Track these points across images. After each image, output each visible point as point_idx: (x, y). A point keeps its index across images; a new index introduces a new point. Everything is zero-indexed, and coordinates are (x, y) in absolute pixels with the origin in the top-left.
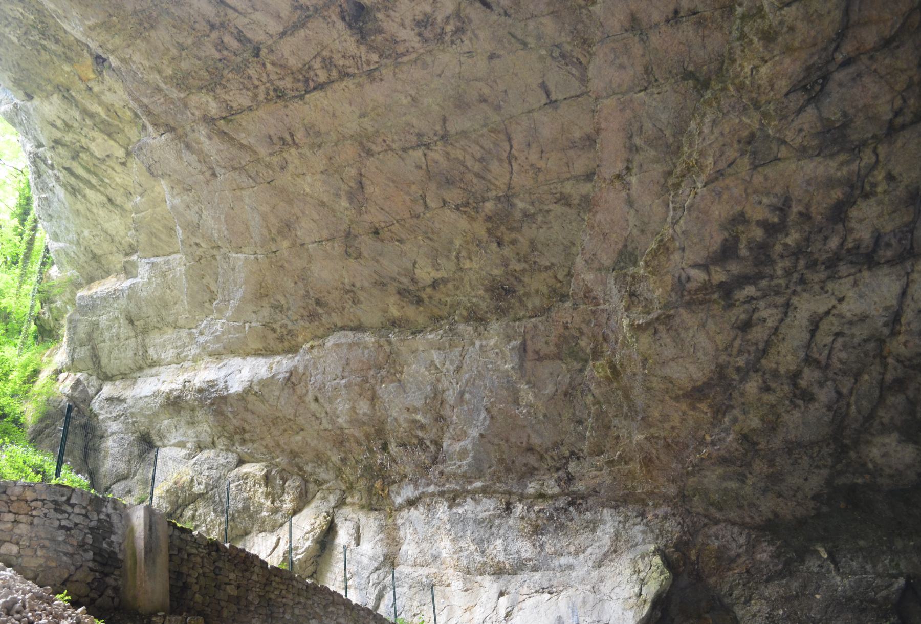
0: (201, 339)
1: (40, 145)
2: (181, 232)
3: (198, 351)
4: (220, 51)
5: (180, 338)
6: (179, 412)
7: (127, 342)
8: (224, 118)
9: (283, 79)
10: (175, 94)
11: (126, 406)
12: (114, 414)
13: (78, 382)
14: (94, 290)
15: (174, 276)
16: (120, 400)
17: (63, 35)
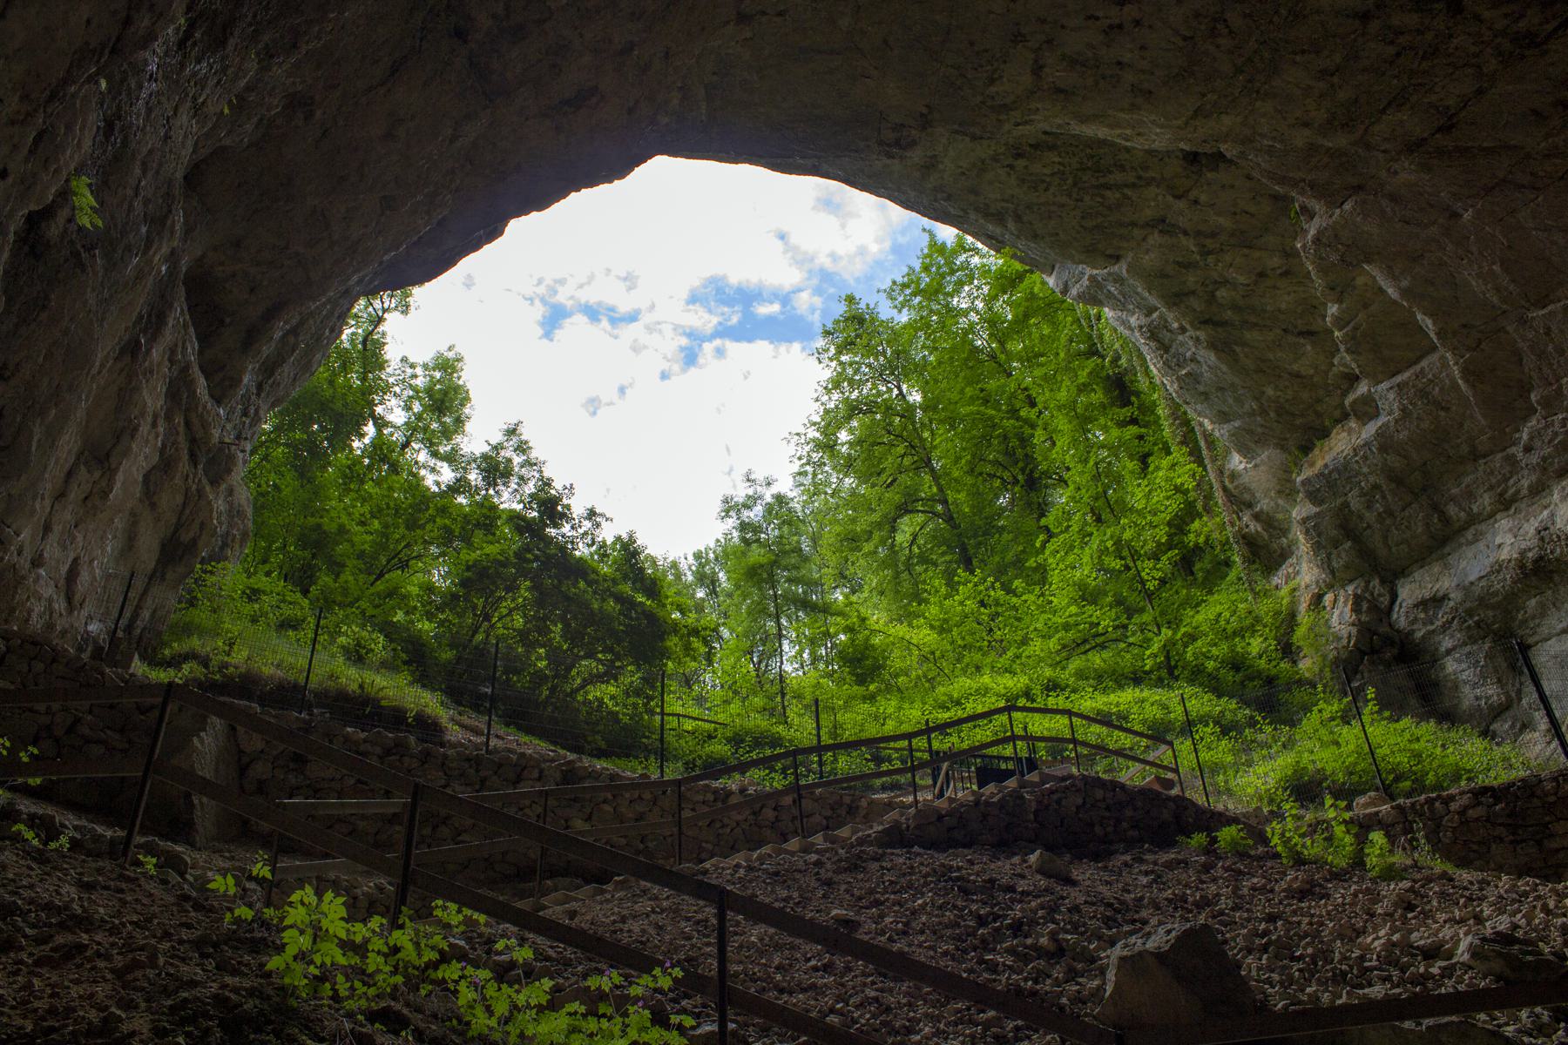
0: (1534, 459)
1: (1150, 311)
2: (1429, 322)
3: (1534, 478)
4: (1392, 43)
5: (1492, 473)
6: (1551, 579)
7: (1407, 513)
8: (1439, 130)
9: (1522, 16)
10: (1341, 141)
11: (1452, 604)
12: (1439, 623)
13: (1358, 600)
14: (1320, 464)
15: (1442, 389)
16: (1438, 601)
17: (1127, 156)
